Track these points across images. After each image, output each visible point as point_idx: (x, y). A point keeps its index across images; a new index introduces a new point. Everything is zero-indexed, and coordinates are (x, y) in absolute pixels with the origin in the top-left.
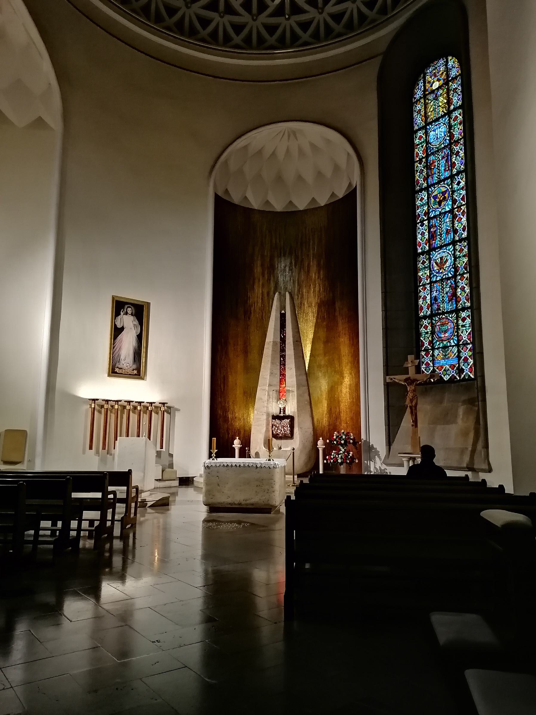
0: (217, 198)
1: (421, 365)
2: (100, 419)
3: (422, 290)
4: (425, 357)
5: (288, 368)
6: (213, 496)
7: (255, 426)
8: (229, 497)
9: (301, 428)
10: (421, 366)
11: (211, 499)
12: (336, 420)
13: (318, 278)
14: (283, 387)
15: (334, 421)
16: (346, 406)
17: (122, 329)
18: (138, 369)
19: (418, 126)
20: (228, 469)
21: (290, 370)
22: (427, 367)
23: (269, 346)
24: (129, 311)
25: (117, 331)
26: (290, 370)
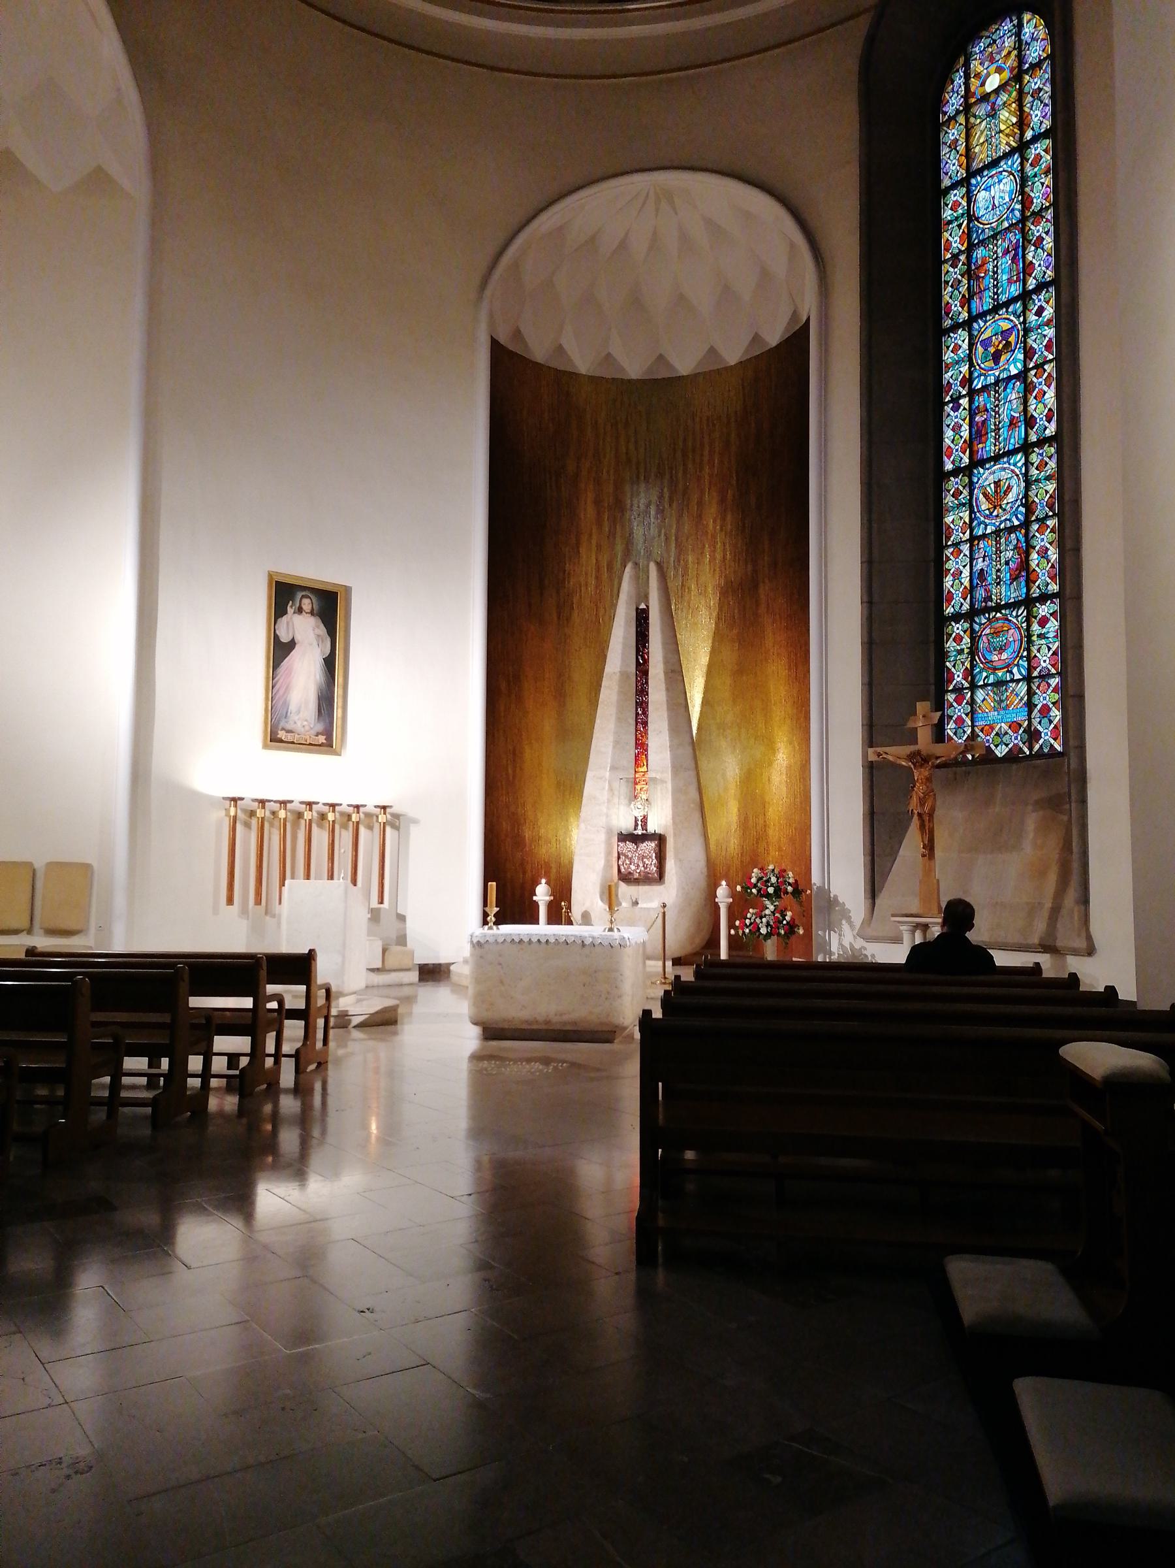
2: (247, 840)
4: (955, 704)
12: (757, 843)
13: (721, 530)
15: (753, 844)
17: (291, 645)
18: (328, 733)
19: (950, 178)
24: (306, 604)
25: (281, 650)
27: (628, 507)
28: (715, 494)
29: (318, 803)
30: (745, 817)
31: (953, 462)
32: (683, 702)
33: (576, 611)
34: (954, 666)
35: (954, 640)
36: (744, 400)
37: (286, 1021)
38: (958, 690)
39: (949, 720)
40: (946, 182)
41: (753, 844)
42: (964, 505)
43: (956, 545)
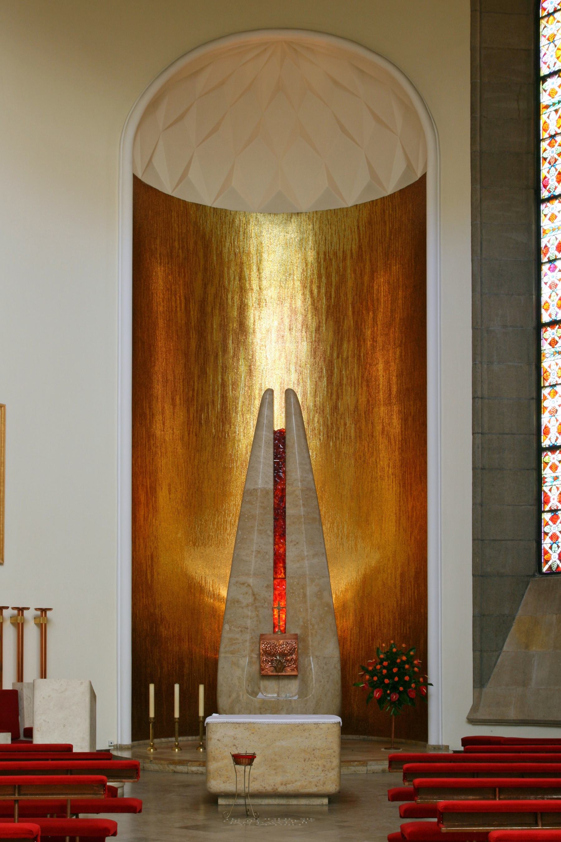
0: (137, 183)
1: (543, 538)
3: (548, 397)
4: (550, 523)
5: (291, 541)
6: (228, 777)
7: (226, 652)
8: (257, 780)
9: (317, 657)
10: (543, 541)
11: (224, 782)
12: (373, 640)
13: (338, 357)
14: (280, 578)
15: (369, 641)
16: (394, 613)
19: (549, 67)
20: (253, 733)
21: (295, 545)
22: (553, 543)
23: (253, 498)
26: (295, 545)
28: (331, 323)
29: (7, 608)
30: (361, 618)
31: (550, 315)
33: (204, 428)
34: (550, 490)
35: (551, 468)
36: (359, 241)
37: (433, 740)
39: (546, 536)
40: (544, 71)
41: (369, 641)
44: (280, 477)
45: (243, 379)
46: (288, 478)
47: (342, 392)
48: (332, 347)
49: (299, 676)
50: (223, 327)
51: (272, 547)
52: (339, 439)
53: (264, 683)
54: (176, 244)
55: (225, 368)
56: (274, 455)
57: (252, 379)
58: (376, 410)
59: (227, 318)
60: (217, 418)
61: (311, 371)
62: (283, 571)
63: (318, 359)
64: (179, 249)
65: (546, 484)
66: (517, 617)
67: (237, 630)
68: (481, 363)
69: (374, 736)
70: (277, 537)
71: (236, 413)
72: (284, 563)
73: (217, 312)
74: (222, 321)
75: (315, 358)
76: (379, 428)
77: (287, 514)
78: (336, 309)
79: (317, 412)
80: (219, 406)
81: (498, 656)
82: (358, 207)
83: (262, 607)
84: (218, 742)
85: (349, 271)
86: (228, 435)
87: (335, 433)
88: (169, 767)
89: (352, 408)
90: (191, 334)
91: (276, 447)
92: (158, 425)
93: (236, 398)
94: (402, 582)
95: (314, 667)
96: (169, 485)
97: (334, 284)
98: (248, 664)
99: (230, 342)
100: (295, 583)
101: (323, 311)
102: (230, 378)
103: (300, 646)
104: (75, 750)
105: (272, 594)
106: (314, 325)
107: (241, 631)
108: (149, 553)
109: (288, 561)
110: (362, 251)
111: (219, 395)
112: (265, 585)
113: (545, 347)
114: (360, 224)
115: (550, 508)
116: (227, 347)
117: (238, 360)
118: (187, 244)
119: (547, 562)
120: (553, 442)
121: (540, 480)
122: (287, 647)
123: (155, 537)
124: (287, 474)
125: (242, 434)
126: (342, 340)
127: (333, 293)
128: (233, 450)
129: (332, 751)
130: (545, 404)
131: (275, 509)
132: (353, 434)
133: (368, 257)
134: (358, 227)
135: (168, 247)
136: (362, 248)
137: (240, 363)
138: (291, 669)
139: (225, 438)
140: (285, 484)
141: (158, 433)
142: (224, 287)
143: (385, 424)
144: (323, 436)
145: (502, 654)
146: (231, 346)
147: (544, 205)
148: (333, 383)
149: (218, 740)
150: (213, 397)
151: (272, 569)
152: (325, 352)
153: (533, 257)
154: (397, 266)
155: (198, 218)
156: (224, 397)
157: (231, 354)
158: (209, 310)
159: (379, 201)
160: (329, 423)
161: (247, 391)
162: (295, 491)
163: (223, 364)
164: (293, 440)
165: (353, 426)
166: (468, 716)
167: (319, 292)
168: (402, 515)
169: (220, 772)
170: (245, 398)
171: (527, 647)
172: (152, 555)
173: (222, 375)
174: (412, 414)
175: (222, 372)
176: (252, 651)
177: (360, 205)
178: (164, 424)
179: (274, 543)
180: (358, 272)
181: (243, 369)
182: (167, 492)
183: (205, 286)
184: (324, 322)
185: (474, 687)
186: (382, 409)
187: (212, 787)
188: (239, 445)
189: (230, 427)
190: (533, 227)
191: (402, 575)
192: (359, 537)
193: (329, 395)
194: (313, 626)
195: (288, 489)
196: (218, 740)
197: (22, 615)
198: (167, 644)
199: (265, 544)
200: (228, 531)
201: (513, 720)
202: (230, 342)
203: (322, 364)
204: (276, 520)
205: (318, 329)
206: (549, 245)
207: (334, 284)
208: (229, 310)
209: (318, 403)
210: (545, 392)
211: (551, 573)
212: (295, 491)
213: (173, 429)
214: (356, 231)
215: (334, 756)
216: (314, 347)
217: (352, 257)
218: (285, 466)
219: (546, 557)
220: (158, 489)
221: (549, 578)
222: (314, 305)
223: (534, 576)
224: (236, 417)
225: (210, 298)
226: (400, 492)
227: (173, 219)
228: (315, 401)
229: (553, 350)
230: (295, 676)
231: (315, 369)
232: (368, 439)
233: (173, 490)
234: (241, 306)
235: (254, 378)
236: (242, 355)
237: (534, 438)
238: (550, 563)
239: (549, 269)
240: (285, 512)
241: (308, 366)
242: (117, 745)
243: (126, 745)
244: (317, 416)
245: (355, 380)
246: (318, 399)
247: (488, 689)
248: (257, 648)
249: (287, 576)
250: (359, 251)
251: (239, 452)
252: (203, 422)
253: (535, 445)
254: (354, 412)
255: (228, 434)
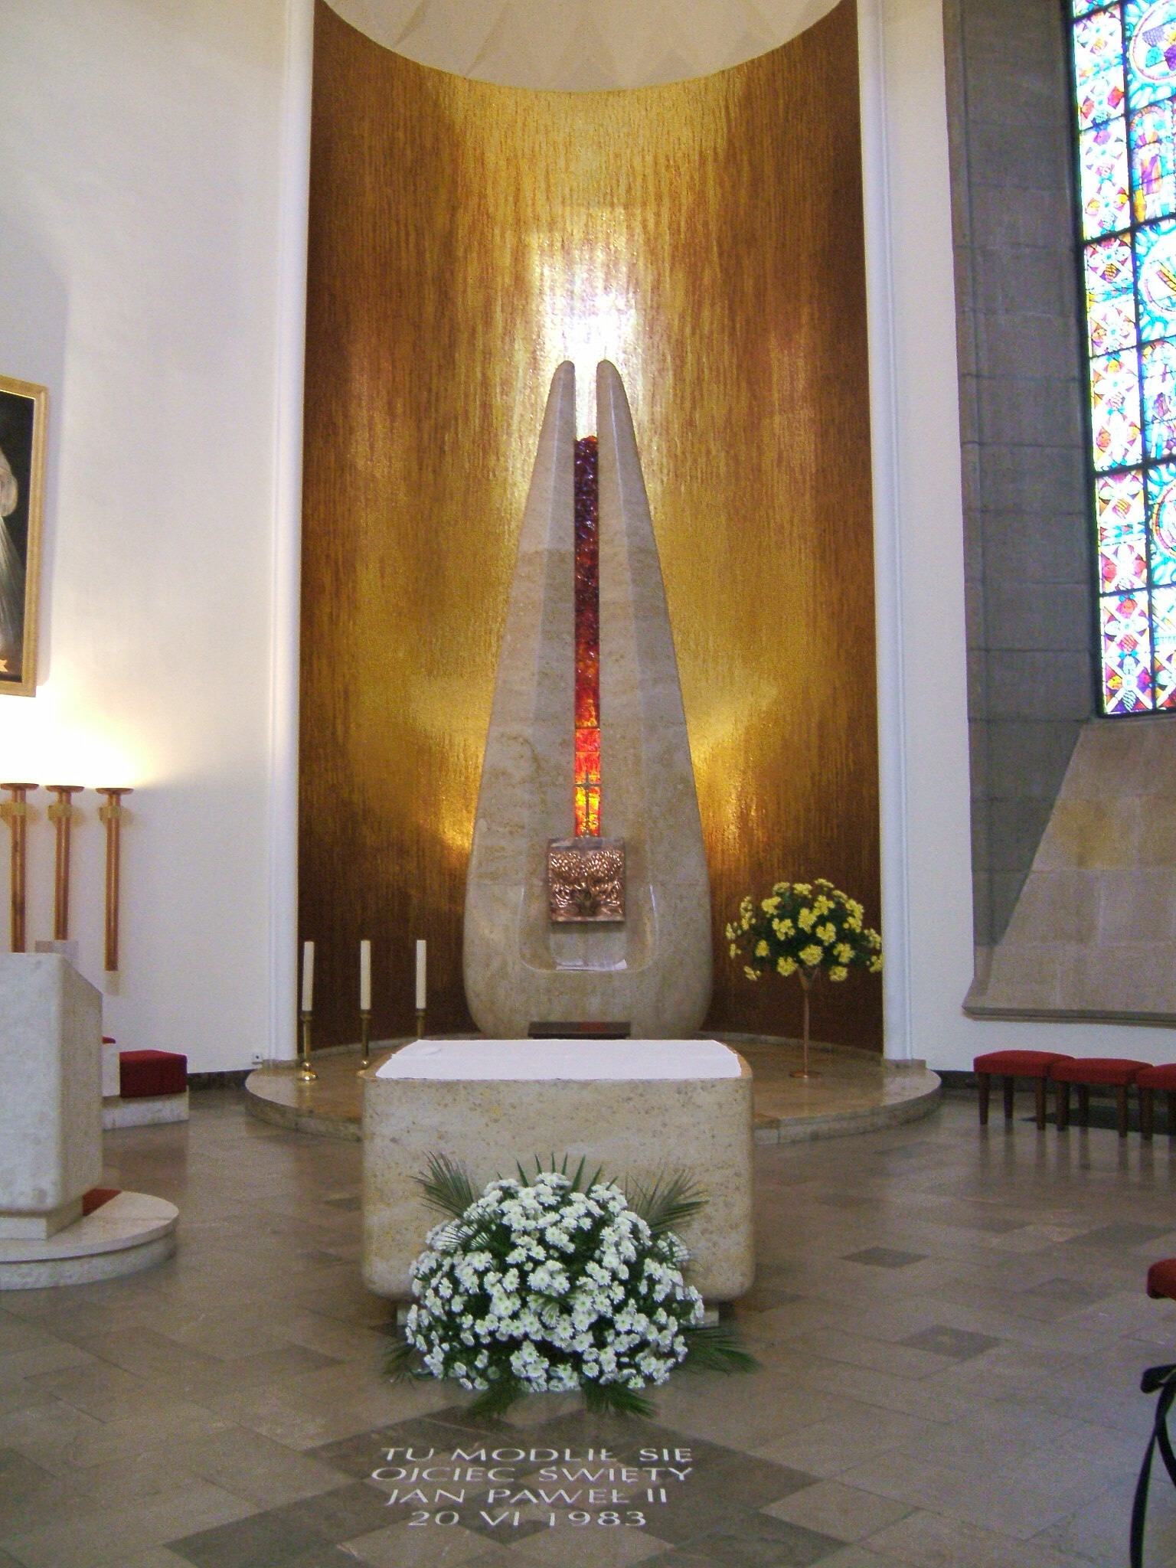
4: (1117, 615)
13: (693, 333)
14: (588, 727)
23: (535, 570)
27: (710, 167)
32: (1081, 506)
33: (449, 459)
34: (1116, 553)
36: (729, 131)
38: (1125, 594)
42: (1124, 290)
43: (1113, 354)
44: (588, 531)
45: (521, 373)
46: (602, 529)
47: (702, 395)
48: (682, 317)
49: (629, 925)
50: (485, 283)
51: (572, 665)
52: (697, 478)
53: (555, 939)
54: (401, 134)
55: (488, 354)
56: (576, 487)
57: (538, 374)
58: (766, 422)
59: (493, 268)
60: (474, 443)
61: (645, 361)
62: (594, 713)
63: (657, 338)
64: (405, 144)
65: (1105, 541)
66: (1058, 803)
67: (501, 830)
68: (974, 311)
69: (770, 1035)
70: (582, 647)
71: (509, 435)
72: (596, 696)
73: (474, 255)
74: (482, 272)
75: (651, 338)
76: (770, 456)
77: (601, 600)
78: (689, 250)
79: (656, 432)
80: (477, 421)
81: (1024, 881)
82: (726, 75)
83: (554, 784)
84: (392, 1145)
85: (711, 183)
86: (495, 476)
87: (690, 469)
88: (346, 1128)
89: (720, 422)
90: (426, 292)
91: (580, 472)
92: (360, 449)
93: (508, 410)
94: (821, 737)
95: (658, 905)
96: (382, 561)
97: (684, 208)
98: (525, 900)
99: (499, 309)
100: (618, 736)
101: (666, 255)
102: (497, 372)
103: (629, 863)
104: (191, 1069)
105: (572, 758)
106: (650, 279)
107: (511, 833)
108: (340, 686)
109: (602, 693)
110: (734, 148)
111: (478, 403)
112: (559, 740)
113: (1092, 280)
114: (730, 102)
115: (1117, 587)
116: (492, 318)
117: (513, 340)
118: (420, 136)
119: (1113, 693)
120: (1119, 460)
121: (1092, 535)
122: (603, 864)
123: (353, 656)
124: (600, 523)
125: (519, 472)
126: (700, 304)
127: (683, 224)
128: (502, 501)
129: (729, 1172)
130: (1094, 389)
131: (578, 592)
132: (723, 470)
133: (745, 158)
134: (727, 108)
135: (385, 137)
136: (733, 144)
137: (516, 347)
138: (610, 910)
139: (488, 480)
140: (596, 543)
141: (360, 463)
142: (487, 214)
143: (782, 447)
144: (668, 475)
145: (1032, 876)
146: (499, 316)
147: (1081, 26)
148: (684, 380)
149: (394, 1140)
150: (466, 404)
151: (573, 709)
152: (669, 326)
153: (1062, 121)
154: (801, 166)
155: (442, 95)
156: (486, 407)
157: (500, 330)
158: (460, 253)
159: (763, 59)
160: (679, 450)
161: (529, 396)
162: (615, 555)
163: (484, 346)
164: (609, 458)
165: (723, 454)
166: (966, 1002)
167: (657, 224)
168: (819, 611)
169: (398, 1237)
170: (525, 407)
171: (1081, 861)
172: (346, 692)
173: (483, 368)
174: (837, 421)
175: (483, 362)
176: (532, 873)
177: (729, 70)
178: (372, 447)
179: (576, 658)
180: (728, 185)
181: (521, 356)
182: (378, 574)
183: (453, 210)
184: (667, 274)
185: (976, 943)
186: (777, 419)
187: (376, 1278)
188: (514, 493)
189: (498, 459)
190: (1061, 65)
191: (821, 725)
192: (736, 656)
193: (678, 401)
194: (655, 822)
195: (604, 551)
196: (394, 1140)
197: (69, 801)
198: (377, 859)
199: (557, 660)
200: (494, 650)
201: (1062, 1011)
202: (499, 309)
203: (665, 347)
204: (579, 612)
205: (656, 287)
206: (1092, 97)
207: (684, 208)
208: (497, 254)
209: (658, 417)
210: (1095, 366)
211: (1123, 715)
212: (615, 555)
213: (390, 458)
214: (723, 115)
215: (738, 1188)
216: (650, 317)
217: (715, 160)
218: (596, 509)
219: (1111, 684)
220: (358, 567)
221: (1122, 723)
222: (649, 246)
223: (1087, 721)
224: (508, 444)
225: (461, 233)
226: (815, 568)
227: (394, 93)
228: (653, 414)
229: (1109, 287)
230: (618, 925)
231: (652, 357)
232: (751, 477)
233: (389, 570)
234: (518, 247)
235: (542, 373)
236: (519, 334)
237: (1078, 455)
238: (1119, 696)
239: (1096, 139)
240: (597, 596)
241: (640, 350)
242: (268, 1060)
243: (285, 1062)
244: (656, 439)
245: (725, 371)
246: (658, 409)
247: (1008, 947)
248: (542, 868)
249: (601, 722)
250: (729, 149)
251: (515, 505)
252: (446, 448)
253: (1080, 467)
254: (725, 428)
255: (494, 473)
